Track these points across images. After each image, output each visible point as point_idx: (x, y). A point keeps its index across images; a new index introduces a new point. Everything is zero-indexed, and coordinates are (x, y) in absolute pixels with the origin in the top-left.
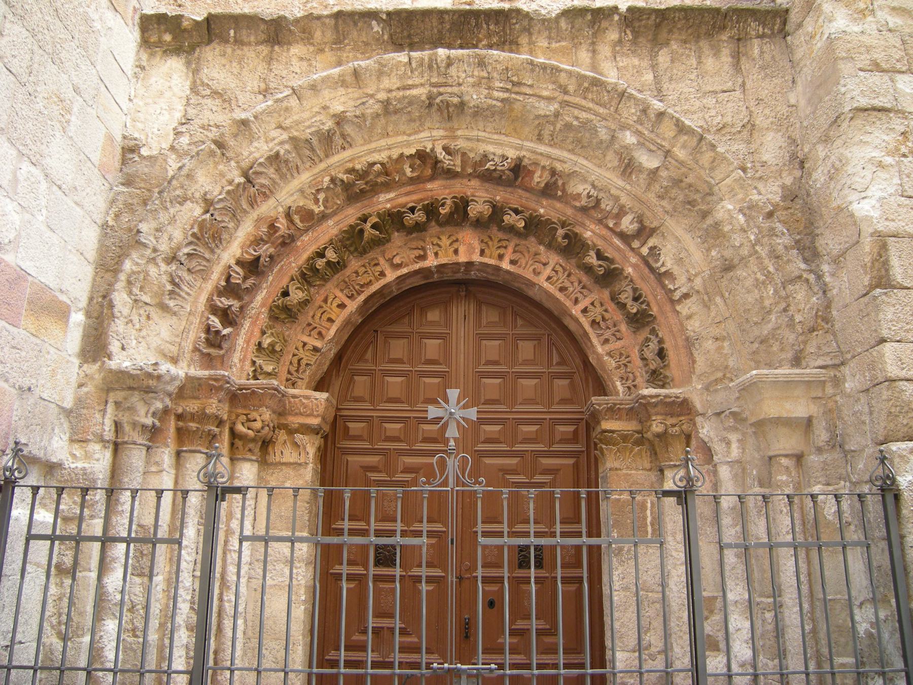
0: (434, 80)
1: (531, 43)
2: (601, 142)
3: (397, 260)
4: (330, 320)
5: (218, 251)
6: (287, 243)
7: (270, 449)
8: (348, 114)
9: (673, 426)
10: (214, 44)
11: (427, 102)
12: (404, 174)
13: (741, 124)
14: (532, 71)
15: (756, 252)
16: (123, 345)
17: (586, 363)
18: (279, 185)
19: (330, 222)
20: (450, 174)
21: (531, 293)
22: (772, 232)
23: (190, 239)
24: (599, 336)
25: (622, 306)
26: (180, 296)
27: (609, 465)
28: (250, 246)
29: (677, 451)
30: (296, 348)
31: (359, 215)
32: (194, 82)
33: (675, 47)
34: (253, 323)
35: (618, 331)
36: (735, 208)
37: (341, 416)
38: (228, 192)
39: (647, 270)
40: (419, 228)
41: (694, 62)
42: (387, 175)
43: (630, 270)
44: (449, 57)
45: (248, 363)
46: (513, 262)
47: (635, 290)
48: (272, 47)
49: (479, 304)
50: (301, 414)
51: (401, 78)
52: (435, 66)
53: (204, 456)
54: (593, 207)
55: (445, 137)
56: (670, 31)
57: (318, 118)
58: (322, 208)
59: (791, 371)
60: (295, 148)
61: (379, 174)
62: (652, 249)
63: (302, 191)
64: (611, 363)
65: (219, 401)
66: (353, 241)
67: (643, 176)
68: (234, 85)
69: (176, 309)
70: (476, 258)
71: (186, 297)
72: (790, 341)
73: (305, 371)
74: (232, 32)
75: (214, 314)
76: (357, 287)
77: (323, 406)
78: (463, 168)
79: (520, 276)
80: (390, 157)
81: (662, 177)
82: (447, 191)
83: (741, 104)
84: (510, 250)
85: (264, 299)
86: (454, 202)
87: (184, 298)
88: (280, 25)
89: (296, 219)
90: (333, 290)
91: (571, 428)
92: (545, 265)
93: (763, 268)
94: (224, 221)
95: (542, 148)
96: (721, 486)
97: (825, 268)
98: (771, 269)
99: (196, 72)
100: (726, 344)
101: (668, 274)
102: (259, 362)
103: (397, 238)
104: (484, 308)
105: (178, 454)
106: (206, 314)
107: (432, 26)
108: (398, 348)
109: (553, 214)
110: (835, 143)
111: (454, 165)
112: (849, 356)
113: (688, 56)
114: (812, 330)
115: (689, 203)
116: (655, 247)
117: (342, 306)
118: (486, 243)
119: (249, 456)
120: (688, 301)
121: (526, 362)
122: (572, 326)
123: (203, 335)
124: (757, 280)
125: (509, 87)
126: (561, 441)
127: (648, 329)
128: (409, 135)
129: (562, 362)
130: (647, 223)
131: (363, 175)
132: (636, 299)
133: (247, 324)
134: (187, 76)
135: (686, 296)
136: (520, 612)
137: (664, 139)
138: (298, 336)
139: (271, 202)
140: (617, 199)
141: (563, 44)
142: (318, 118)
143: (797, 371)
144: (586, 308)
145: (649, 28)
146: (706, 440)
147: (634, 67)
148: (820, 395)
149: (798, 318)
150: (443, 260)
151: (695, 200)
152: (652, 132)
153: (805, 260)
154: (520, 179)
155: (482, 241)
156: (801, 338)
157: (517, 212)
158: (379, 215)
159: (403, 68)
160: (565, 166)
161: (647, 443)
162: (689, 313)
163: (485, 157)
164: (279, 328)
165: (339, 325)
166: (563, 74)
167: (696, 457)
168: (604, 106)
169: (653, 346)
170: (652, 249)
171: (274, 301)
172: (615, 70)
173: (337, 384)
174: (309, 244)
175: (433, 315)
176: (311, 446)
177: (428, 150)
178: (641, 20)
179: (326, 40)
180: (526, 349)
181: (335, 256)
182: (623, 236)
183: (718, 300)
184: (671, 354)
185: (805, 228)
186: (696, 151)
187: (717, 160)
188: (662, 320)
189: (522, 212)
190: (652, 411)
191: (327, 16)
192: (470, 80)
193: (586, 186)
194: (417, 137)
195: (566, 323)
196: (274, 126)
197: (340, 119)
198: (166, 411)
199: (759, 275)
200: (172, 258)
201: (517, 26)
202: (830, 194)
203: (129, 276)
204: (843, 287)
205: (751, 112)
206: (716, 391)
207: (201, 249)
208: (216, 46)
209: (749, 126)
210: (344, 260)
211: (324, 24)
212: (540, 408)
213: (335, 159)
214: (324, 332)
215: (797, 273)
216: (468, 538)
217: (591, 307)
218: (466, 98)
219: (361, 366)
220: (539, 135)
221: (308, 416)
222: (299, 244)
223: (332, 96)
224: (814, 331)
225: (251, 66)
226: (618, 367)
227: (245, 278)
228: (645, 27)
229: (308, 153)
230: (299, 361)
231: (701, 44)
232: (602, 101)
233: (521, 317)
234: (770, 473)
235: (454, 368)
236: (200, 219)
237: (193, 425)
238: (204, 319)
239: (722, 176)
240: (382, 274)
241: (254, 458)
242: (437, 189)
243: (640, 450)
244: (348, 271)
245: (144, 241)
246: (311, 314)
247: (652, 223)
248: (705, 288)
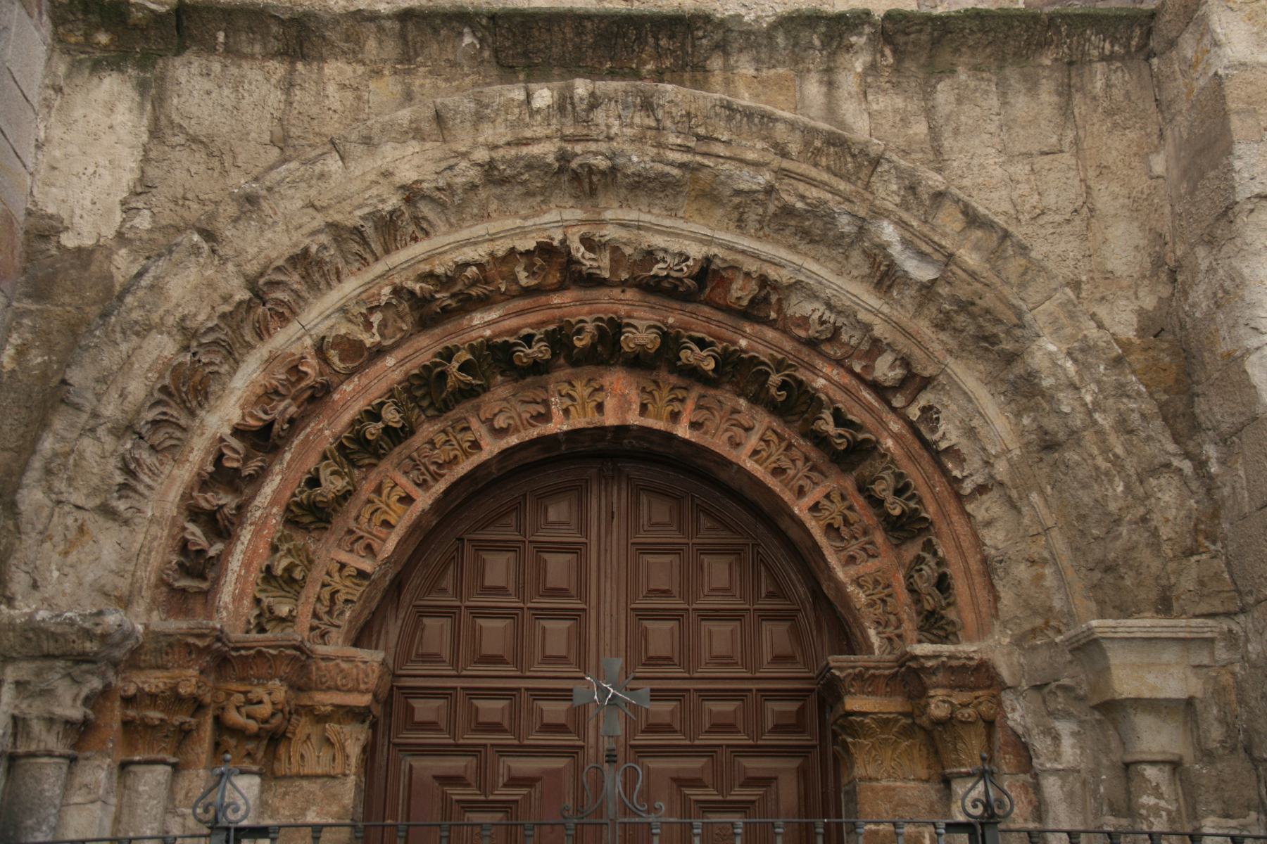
0: (569, 131)
1: (727, 68)
2: (842, 235)
3: (500, 422)
4: (386, 524)
5: (202, 413)
6: (319, 396)
7: (282, 750)
8: (425, 185)
9: (965, 705)
10: (188, 55)
11: (557, 165)
12: (515, 280)
13: (1071, 208)
14: (730, 119)
15: (1095, 423)
16: (35, 581)
17: (817, 594)
18: (305, 300)
19: (390, 361)
21: (724, 476)
22: (1122, 391)
23: (157, 395)
24: (838, 550)
25: (876, 502)
26: (136, 491)
27: (859, 771)
28: (256, 403)
29: (972, 748)
30: (328, 574)
31: (439, 348)
32: (156, 120)
33: (963, 77)
34: (256, 534)
35: (871, 543)
36: (1059, 349)
37: (399, 688)
38: (223, 316)
39: (917, 445)
40: (538, 368)
41: (994, 102)
42: (487, 283)
43: (890, 443)
44: (592, 94)
45: (247, 602)
46: (694, 425)
47: (899, 476)
48: (293, 63)
50: (338, 689)
51: (512, 126)
52: (569, 107)
53: (169, 768)
54: (828, 340)
55: (584, 222)
56: (957, 51)
57: (374, 191)
58: (377, 338)
59: (1156, 622)
60: (335, 240)
61: (474, 282)
62: (925, 410)
63: (343, 310)
64: (860, 597)
66: (430, 391)
67: (912, 292)
68: (227, 129)
69: (128, 514)
70: (634, 419)
71: (146, 492)
72: (1153, 570)
73: (342, 613)
74: (221, 37)
75: (193, 521)
77: (376, 675)
78: (613, 270)
80: (492, 254)
81: (941, 296)
82: (587, 308)
83: (1071, 174)
84: (690, 405)
85: (277, 492)
86: (598, 327)
87: (142, 495)
88: (307, 28)
89: (334, 356)
90: (392, 474)
92: (748, 430)
93: (1106, 450)
94: (212, 363)
95: (745, 243)
96: (1047, 811)
97: (1211, 451)
98: (1119, 450)
99: (160, 102)
100: (1048, 571)
101: (952, 451)
103: (501, 391)
104: (644, 499)
105: (124, 766)
106: (182, 521)
107: (564, 39)
108: (498, 569)
109: (761, 348)
110: (1225, 249)
111: (599, 268)
112: (1250, 600)
113: (986, 92)
114: (1190, 552)
115: (985, 339)
116: (931, 408)
117: (407, 500)
118: (650, 393)
119: (247, 764)
120: (985, 497)
122: (794, 533)
123: (175, 559)
124: (1097, 468)
125: (692, 144)
126: (777, 729)
127: (920, 542)
128: (525, 218)
130: (918, 369)
131: (444, 282)
132: (898, 492)
133: (246, 535)
134: (141, 106)
135: (981, 489)
137: (944, 235)
138: (331, 552)
139: (293, 328)
140: (867, 327)
141: (781, 70)
142: (374, 191)
143: (1165, 622)
144: (817, 503)
145: (916, 45)
146: (1020, 730)
147: (896, 111)
148: (1206, 661)
149: (1165, 532)
150: (578, 422)
151: (995, 335)
152: (926, 222)
153: (1176, 439)
154: (708, 290)
156: (1172, 566)
157: (702, 344)
158: (472, 348)
159: (517, 111)
160: (784, 272)
162: (987, 517)
163: (650, 255)
164: (299, 539)
165: (401, 533)
166: (780, 126)
167: (1006, 761)
168: (846, 177)
169: (929, 570)
170: (925, 410)
171: (294, 495)
172: (866, 116)
173: (393, 629)
174: (352, 398)
175: (558, 511)
176: (353, 739)
177: (556, 243)
178: (908, 34)
179: (384, 56)
180: (719, 570)
181: (398, 417)
182: (877, 388)
183: (1035, 497)
184: (960, 586)
185: (1177, 381)
186: (994, 256)
187: (1034, 269)
188: (944, 528)
189: (711, 344)
191: (388, 17)
192: (628, 131)
193: (816, 305)
194: (537, 221)
195: (783, 527)
196: (299, 204)
197: (412, 194)
198: (106, 692)
199: (1100, 461)
200: (126, 429)
201: (704, 41)
202: (1217, 330)
203: (49, 461)
204: (1238, 485)
205: (1088, 187)
206: (1034, 648)
207: (173, 412)
208: (193, 58)
209: (1085, 209)
210: (411, 424)
211: (381, 29)
212: (739, 672)
213: (400, 257)
215: (1162, 459)
217: (825, 502)
218: (620, 161)
220: (740, 220)
221: (350, 691)
222: (336, 396)
223: (398, 154)
224: (1192, 554)
225: (256, 95)
226: (872, 604)
227: (246, 459)
228: (915, 44)
229: (356, 247)
230: (334, 594)
231: (1007, 72)
232: (844, 171)
233: (709, 515)
234: (1128, 792)
235: (593, 602)
237: (155, 715)
238: (176, 530)
239: (1038, 297)
240: (476, 445)
241: (255, 768)
242: (565, 302)
244: (417, 440)
245: (76, 400)
246: (354, 514)
247: (925, 369)
248: (1013, 480)
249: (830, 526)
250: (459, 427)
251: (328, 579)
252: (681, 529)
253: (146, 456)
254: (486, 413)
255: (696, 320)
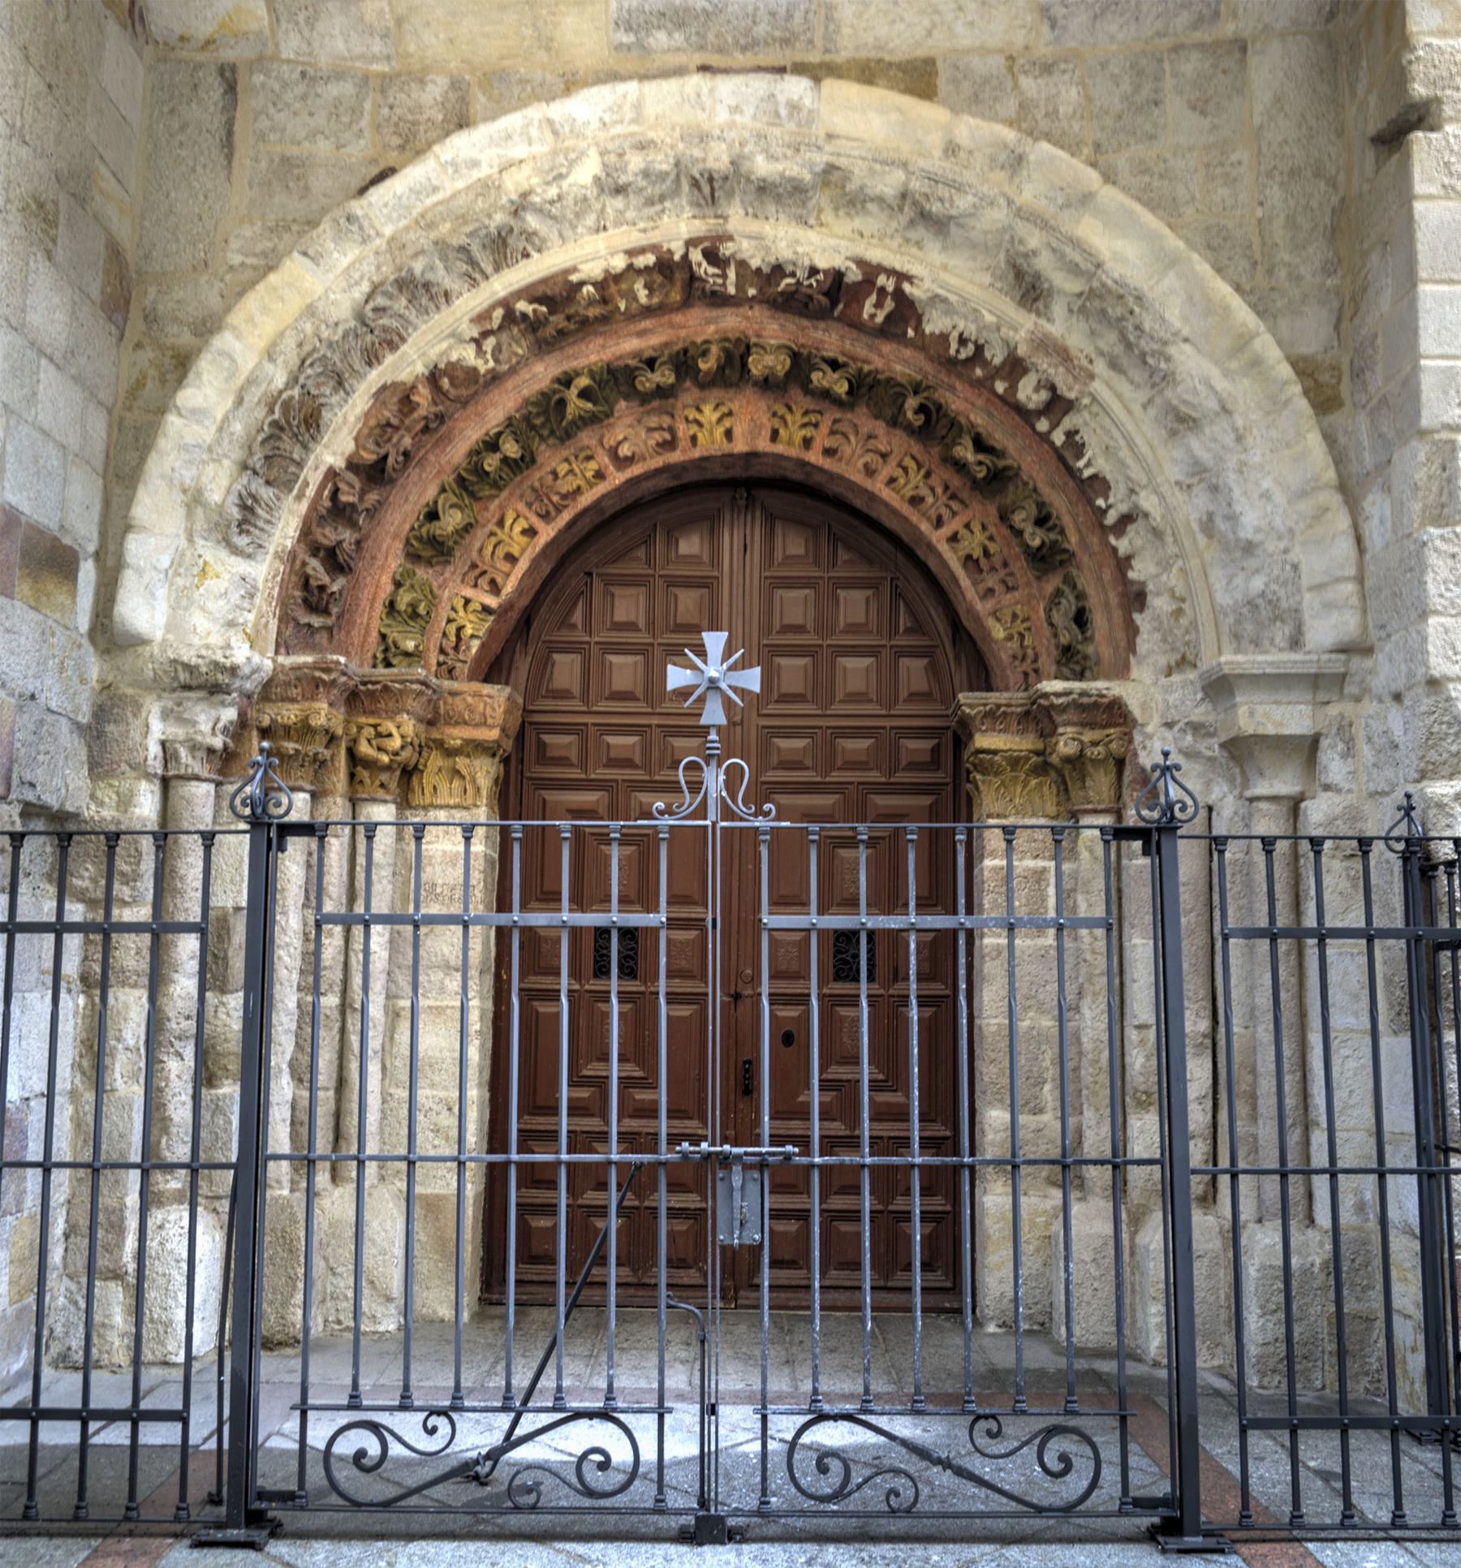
3: (625, 450)
4: (511, 559)
6: (434, 427)
7: (415, 781)
9: (1095, 744)
12: (635, 299)
20: (718, 299)
29: (1100, 784)
35: (1012, 574)
40: (663, 393)
47: (1041, 505)
49: (770, 520)
58: (491, 364)
61: (591, 302)
65: (331, 705)
66: (547, 419)
70: (763, 445)
75: (314, 555)
76: (555, 498)
78: (740, 286)
79: (841, 478)
84: (824, 429)
86: (725, 350)
89: (445, 382)
91: (928, 744)
102: (393, 635)
104: (779, 531)
119: (381, 794)
121: (852, 629)
126: (912, 766)
129: (917, 628)
136: (838, 1052)
155: (775, 414)
157: (834, 365)
158: (592, 374)
161: (1053, 774)
164: (422, 573)
169: (1069, 604)
170: (1070, 434)
173: (523, 667)
175: (690, 545)
176: (484, 772)
180: (854, 605)
182: (1019, 409)
189: (845, 365)
190: (1059, 719)
214: (499, 580)
216: (742, 927)
219: (564, 635)
221: (477, 725)
226: (1010, 638)
233: (848, 547)
236: (284, 396)
237: (290, 746)
243: (1041, 784)
246: (477, 545)
249: (969, 557)
250: (582, 455)
251: (453, 615)
252: (817, 562)
253: (266, 493)
254: (610, 441)
255: (829, 339)
